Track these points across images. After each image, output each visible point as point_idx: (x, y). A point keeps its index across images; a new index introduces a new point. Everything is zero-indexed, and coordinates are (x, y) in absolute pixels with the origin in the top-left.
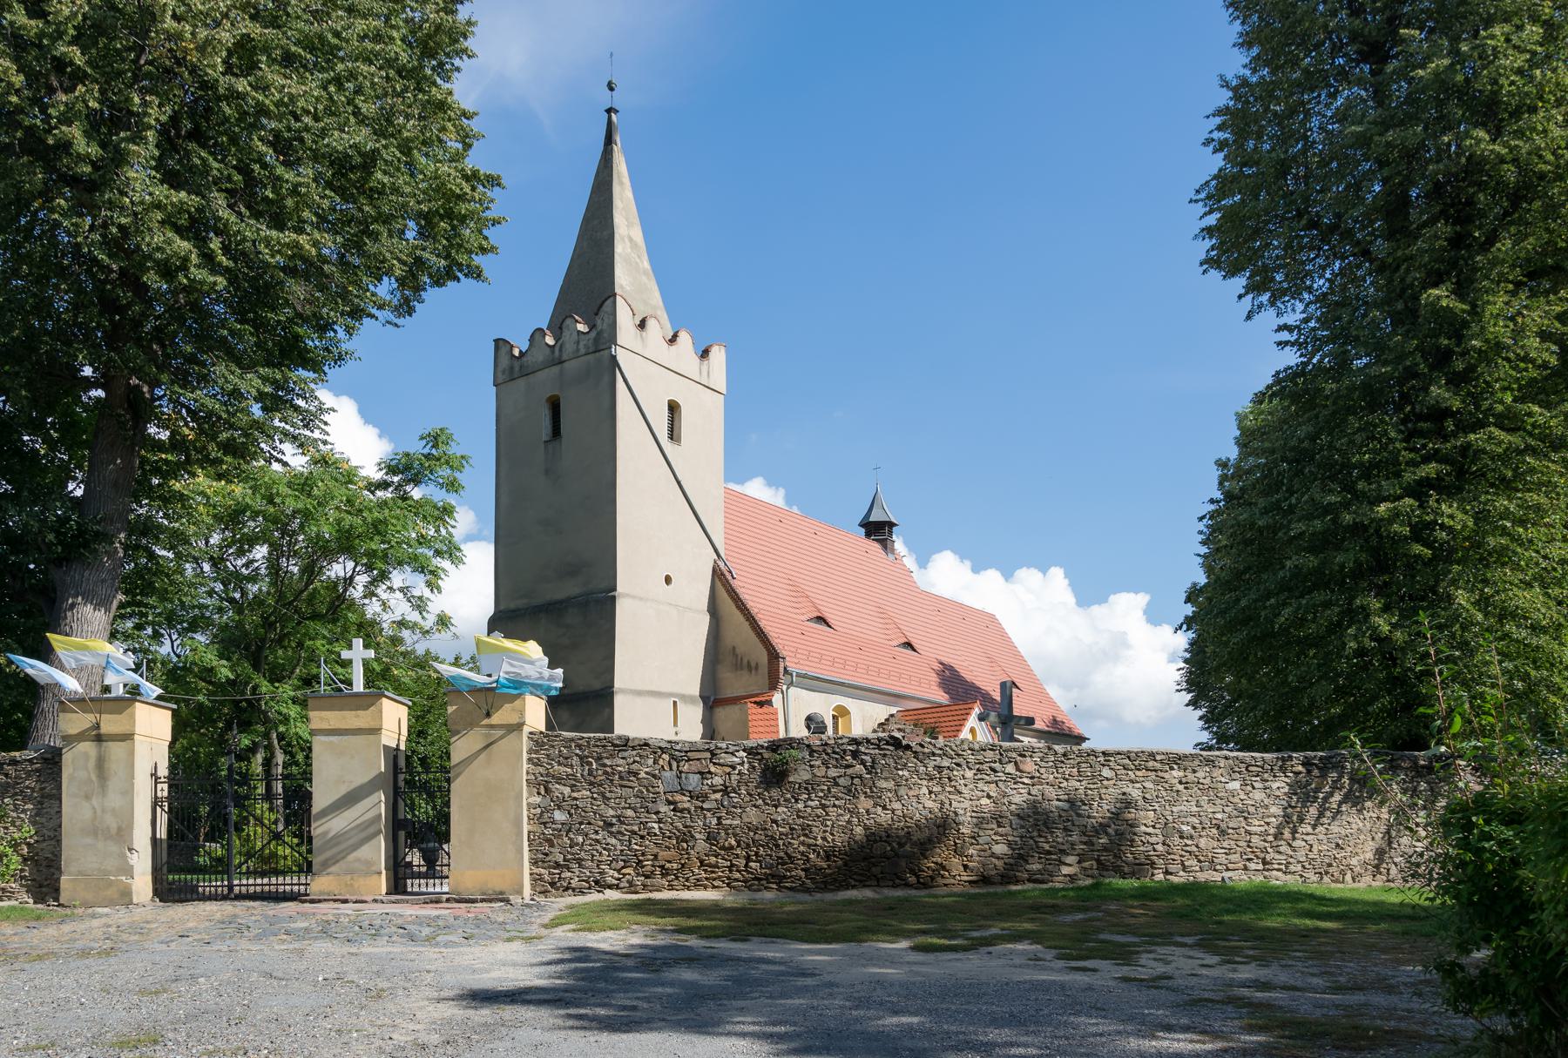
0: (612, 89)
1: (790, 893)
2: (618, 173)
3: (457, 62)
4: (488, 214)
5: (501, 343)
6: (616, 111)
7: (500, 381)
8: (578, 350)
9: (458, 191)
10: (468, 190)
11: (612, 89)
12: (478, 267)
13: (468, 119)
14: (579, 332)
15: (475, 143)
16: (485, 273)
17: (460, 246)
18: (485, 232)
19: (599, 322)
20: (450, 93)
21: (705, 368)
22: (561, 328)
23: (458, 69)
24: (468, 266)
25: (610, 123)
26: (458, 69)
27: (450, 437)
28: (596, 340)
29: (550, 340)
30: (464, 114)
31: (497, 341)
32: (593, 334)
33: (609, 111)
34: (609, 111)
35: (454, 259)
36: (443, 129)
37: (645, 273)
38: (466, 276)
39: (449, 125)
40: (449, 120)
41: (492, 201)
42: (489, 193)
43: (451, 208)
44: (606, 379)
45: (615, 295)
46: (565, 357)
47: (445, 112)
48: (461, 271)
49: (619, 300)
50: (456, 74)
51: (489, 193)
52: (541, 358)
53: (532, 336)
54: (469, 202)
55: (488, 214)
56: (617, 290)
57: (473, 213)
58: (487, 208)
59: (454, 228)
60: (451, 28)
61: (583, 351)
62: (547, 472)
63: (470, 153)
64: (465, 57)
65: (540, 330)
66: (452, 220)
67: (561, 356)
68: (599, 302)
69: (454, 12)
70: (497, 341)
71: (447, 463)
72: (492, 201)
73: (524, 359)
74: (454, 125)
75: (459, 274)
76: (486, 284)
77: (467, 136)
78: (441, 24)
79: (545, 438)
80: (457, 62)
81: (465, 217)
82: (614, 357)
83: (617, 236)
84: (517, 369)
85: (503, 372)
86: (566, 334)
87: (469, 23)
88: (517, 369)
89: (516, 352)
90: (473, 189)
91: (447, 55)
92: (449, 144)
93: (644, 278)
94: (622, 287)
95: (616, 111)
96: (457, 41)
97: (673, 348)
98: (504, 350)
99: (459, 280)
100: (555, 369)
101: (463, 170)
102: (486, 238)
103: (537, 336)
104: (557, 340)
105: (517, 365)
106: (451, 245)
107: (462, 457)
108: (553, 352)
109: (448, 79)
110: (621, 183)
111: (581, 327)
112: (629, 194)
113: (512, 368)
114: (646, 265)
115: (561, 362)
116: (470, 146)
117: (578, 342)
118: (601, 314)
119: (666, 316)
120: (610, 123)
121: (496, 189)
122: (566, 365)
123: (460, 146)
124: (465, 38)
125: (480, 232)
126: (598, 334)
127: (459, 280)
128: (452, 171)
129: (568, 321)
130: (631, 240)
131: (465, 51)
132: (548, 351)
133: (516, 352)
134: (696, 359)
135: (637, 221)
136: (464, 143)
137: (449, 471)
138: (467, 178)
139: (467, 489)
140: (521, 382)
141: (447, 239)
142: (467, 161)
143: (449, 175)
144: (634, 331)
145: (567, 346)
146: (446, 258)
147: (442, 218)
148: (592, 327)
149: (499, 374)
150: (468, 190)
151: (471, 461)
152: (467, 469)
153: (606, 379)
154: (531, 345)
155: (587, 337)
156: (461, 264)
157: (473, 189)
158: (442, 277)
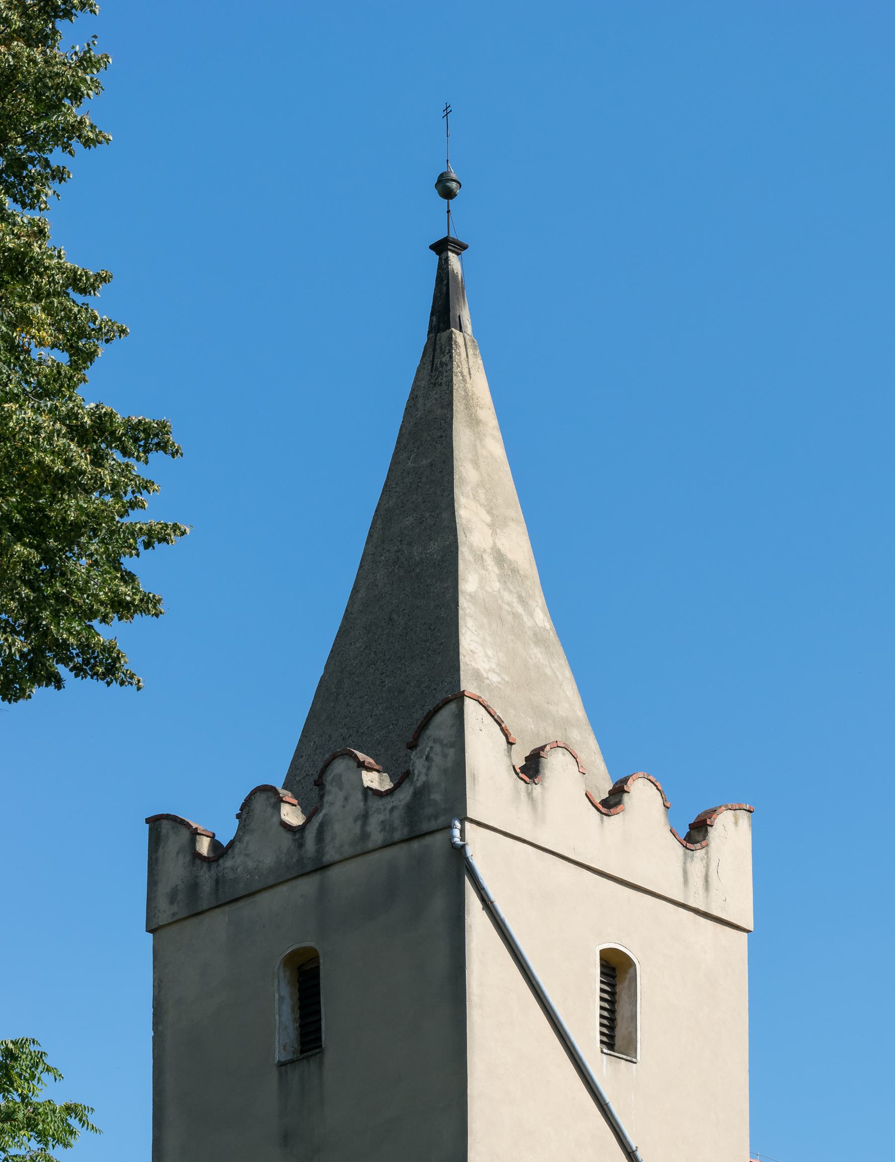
0: (448, 195)
1: (405, 846)
2: (467, 397)
3: (57, 157)
4: (135, 518)
5: (166, 825)
6: (461, 248)
7: (163, 919)
8: (364, 836)
9: (59, 467)
10: (84, 463)
11: (448, 195)
12: (108, 649)
13: (83, 291)
14: (368, 792)
15: (102, 350)
16: (128, 663)
17: (63, 600)
18: (128, 563)
19: (419, 765)
20: (41, 233)
21: (696, 867)
22: (320, 784)
23: (59, 175)
24: (85, 647)
25: (444, 275)
26: (59, 175)
27: (37, 1060)
28: (412, 810)
29: (292, 815)
30: (75, 281)
31: (155, 822)
32: (405, 795)
33: (441, 247)
34: (441, 247)
35: (47, 632)
36: (23, 320)
37: (539, 639)
38: (78, 671)
39: (37, 311)
40: (37, 298)
41: (146, 486)
42: (137, 468)
43: (40, 509)
44: (439, 904)
45: (460, 697)
46: (331, 854)
47: (26, 280)
48: (65, 660)
49: (470, 706)
50: (55, 185)
51: (137, 468)
52: (269, 861)
53: (247, 804)
54: (88, 491)
55: (135, 518)
56: (467, 685)
57: (95, 517)
58: (133, 505)
59: (48, 556)
60: (40, 78)
61: (377, 837)
62: (286, 1138)
63: (88, 373)
64: (75, 144)
65: (267, 790)
66: (44, 537)
67: (320, 851)
68: (419, 715)
69: (45, 39)
70: (155, 822)
71: (31, 1124)
72: (146, 486)
73: (228, 863)
74: (47, 309)
75: (62, 670)
76: (130, 689)
77: (81, 333)
78: (15, 69)
79: (279, 1055)
80: (57, 157)
81: (76, 528)
82: (459, 852)
83: (464, 553)
84: (207, 887)
85: (172, 898)
86: (334, 796)
87: (86, 62)
88: (207, 887)
89: (204, 846)
90: (98, 459)
91: (31, 140)
92: (37, 353)
93: (537, 654)
94: (477, 676)
95: (461, 248)
96: (56, 107)
97: (615, 821)
98: (174, 842)
99: (59, 683)
100: (307, 886)
101: (72, 415)
102: (129, 578)
103: (260, 803)
104: (310, 812)
105: (206, 877)
106: (41, 601)
107: (70, 1109)
108: (301, 845)
109: (29, 201)
110: (474, 422)
111: (372, 780)
112: (488, 414)
113: (193, 887)
114: (541, 618)
115: (322, 868)
116: (90, 356)
117: (365, 817)
118: (425, 745)
119: (593, 743)
120: (444, 275)
121: (156, 456)
122: (334, 873)
123: (63, 358)
124: (77, 96)
125: (115, 564)
126: (418, 794)
127: (59, 683)
128: (44, 420)
129: (340, 766)
130: (500, 558)
131: (75, 129)
132: (287, 840)
133: (204, 846)
134: (676, 849)
135: (515, 512)
136: (73, 350)
137: (34, 1145)
138: (80, 434)
139: (66, 1150)
140: (219, 921)
141: (29, 584)
142: (80, 392)
143: (37, 429)
144: (508, 781)
145: (337, 827)
146: (27, 631)
147: (18, 533)
148: (401, 778)
149: (163, 903)
150: (84, 463)
151: (91, 1118)
152: (83, 1137)
153: (439, 904)
154: (244, 827)
155: (389, 802)
156: (65, 645)
157: (98, 459)
158: (18, 678)
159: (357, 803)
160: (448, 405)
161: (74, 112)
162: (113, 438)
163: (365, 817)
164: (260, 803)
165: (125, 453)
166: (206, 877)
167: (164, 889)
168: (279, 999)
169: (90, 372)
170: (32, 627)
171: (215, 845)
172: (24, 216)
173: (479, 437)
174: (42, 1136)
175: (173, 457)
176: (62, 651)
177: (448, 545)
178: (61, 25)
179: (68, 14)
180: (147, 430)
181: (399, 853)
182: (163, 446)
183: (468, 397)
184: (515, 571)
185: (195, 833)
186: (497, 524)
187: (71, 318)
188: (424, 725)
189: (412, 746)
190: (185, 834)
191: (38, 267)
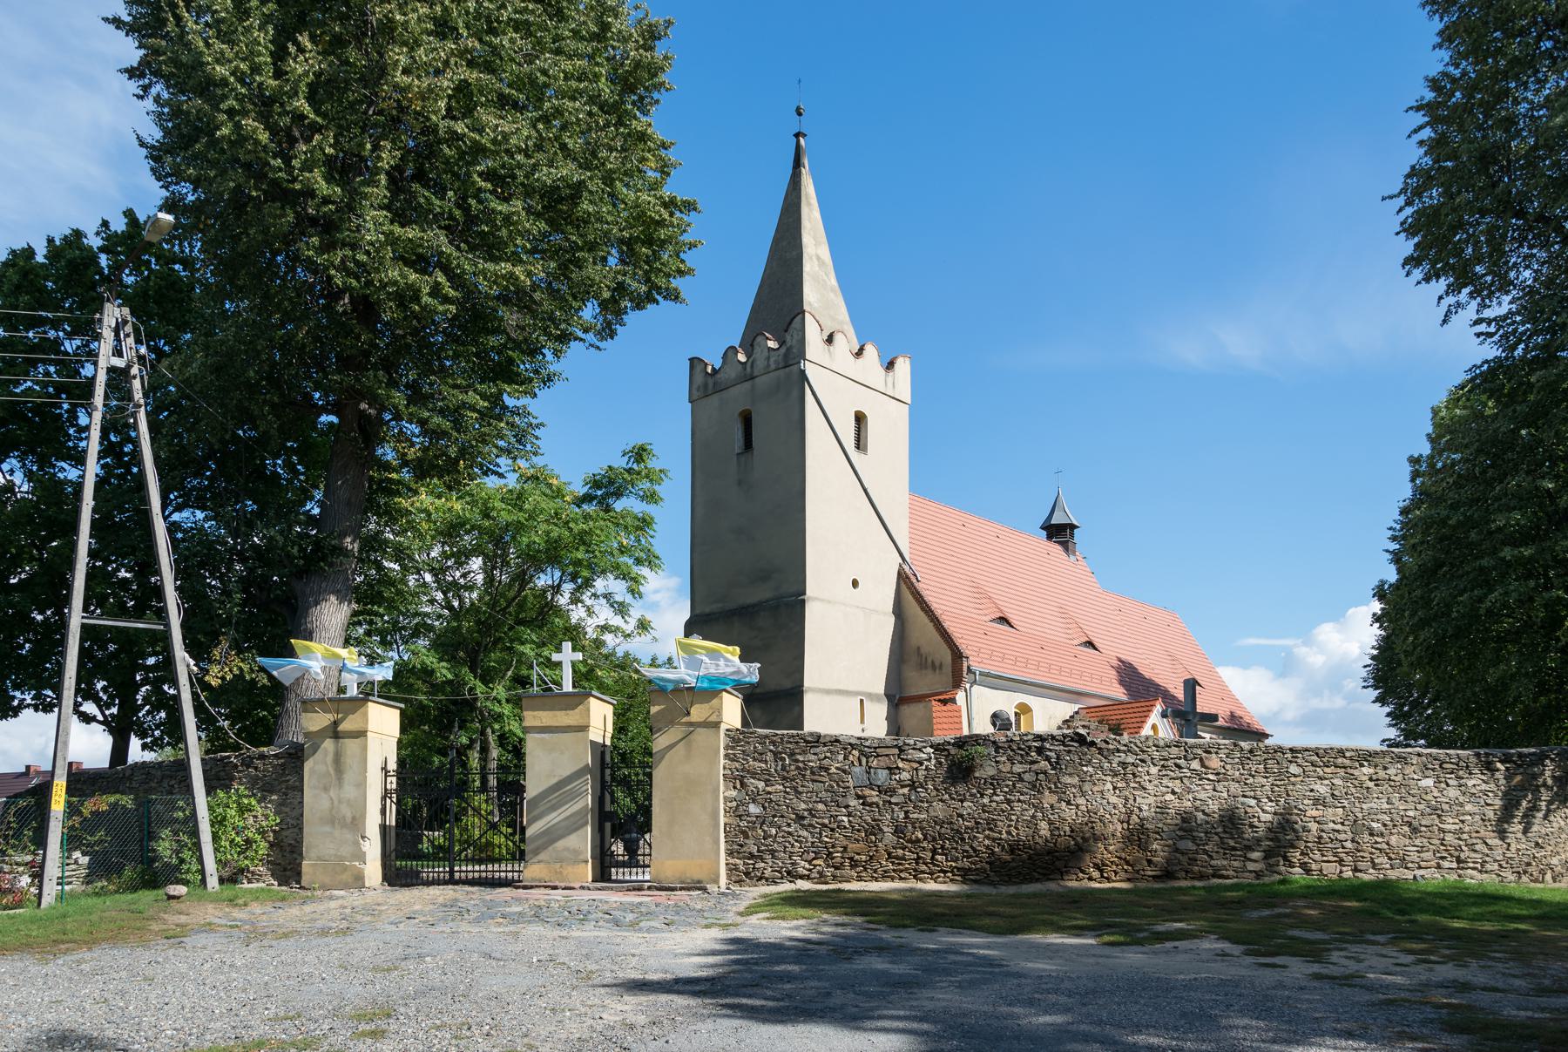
0: (800, 114)
6: (804, 135)
7: (695, 398)
8: (768, 365)
10: (666, 216)
11: (800, 114)
12: (676, 289)
14: (770, 349)
16: (683, 295)
19: (788, 338)
21: (890, 379)
22: (752, 345)
28: (786, 356)
29: (742, 358)
30: (664, 146)
31: (692, 360)
32: (783, 350)
33: (797, 135)
34: (797, 135)
37: (832, 290)
38: (665, 298)
44: (795, 393)
48: (659, 294)
52: (733, 375)
56: (805, 307)
60: (649, 64)
61: (773, 366)
62: (740, 483)
65: (732, 348)
68: (788, 319)
69: (651, 49)
70: (692, 360)
71: (647, 476)
73: (718, 376)
75: (658, 297)
77: (665, 166)
80: (656, 95)
82: (803, 372)
86: (757, 350)
87: (666, 58)
89: (709, 369)
90: (672, 215)
91: (646, 89)
93: (832, 295)
94: (810, 304)
95: (804, 135)
96: (656, 75)
98: (699, 368)
99: (658, 303)
100: (747, 385)
101: (661, 197)
102: (683, 261)
103: (730, 353)
104: (749, 356)
105: (710, 381)
106: (650, 271)
109: (646, 113)
110: (809, 204)
111: (772, 344)
112: (814, 201)
113: (706, 385)
114: (833, 282)
115: (753, 378)
117: (768, 358)
118: (790, 331)
120: (798, 146)
121: (692, 213)
126: (788, 350)
127: (658, 303)
129: (759, 339)
130: (818, 258)
131: (662, 84)
133: (709, 369)
134: (883, 372)
137: (648, 484)
138: (665, 205)
140: (715, 397)
149: (695, 392)
150: (666, 216)
151: (669, 474)
154: (724, 363)
156: (660, 288)
157: (672, 215)
159: (766, 353)
160: (799, 197)
161: (662, 78)
162: (676, 206)
163: (768, 358)
164: (730, 353)
165: (681, 212)
166: (710, 381)
167: (695, 386)
168: (718, 876)
169: (669, 180)
170: (648, 280)
171: (713, 369)
172: (644, 119)
173: (811, 210)
174: (651, 480)
175: (1128, 675)
176: (659, 289)
177: (196, 375)
178: (657, 43)
179: (659, 39)
180: (689, 203)
181: (781, 372)
182: (695, 209)
183: (807, 195)
184: (824, 263)
185: (706, 364)
186: (817, 244)
187: (662, 159)
188: (790, 323)
189: (786, 331)
190: (703, 365)
191: (650, 138)
